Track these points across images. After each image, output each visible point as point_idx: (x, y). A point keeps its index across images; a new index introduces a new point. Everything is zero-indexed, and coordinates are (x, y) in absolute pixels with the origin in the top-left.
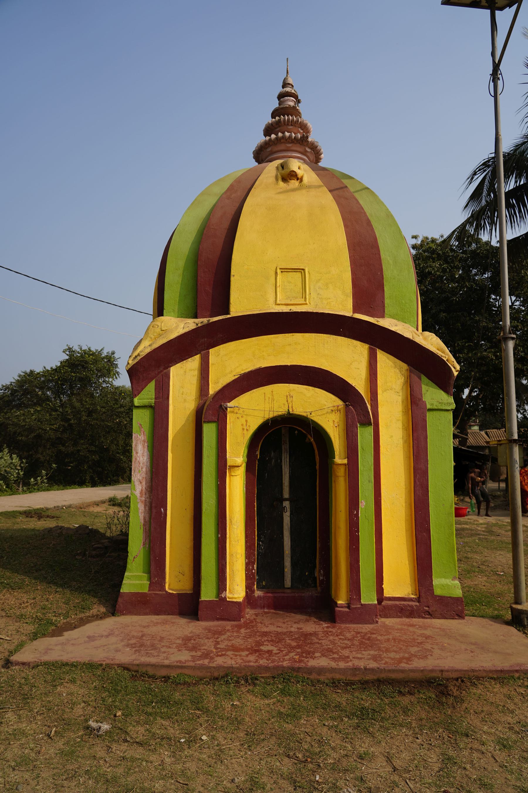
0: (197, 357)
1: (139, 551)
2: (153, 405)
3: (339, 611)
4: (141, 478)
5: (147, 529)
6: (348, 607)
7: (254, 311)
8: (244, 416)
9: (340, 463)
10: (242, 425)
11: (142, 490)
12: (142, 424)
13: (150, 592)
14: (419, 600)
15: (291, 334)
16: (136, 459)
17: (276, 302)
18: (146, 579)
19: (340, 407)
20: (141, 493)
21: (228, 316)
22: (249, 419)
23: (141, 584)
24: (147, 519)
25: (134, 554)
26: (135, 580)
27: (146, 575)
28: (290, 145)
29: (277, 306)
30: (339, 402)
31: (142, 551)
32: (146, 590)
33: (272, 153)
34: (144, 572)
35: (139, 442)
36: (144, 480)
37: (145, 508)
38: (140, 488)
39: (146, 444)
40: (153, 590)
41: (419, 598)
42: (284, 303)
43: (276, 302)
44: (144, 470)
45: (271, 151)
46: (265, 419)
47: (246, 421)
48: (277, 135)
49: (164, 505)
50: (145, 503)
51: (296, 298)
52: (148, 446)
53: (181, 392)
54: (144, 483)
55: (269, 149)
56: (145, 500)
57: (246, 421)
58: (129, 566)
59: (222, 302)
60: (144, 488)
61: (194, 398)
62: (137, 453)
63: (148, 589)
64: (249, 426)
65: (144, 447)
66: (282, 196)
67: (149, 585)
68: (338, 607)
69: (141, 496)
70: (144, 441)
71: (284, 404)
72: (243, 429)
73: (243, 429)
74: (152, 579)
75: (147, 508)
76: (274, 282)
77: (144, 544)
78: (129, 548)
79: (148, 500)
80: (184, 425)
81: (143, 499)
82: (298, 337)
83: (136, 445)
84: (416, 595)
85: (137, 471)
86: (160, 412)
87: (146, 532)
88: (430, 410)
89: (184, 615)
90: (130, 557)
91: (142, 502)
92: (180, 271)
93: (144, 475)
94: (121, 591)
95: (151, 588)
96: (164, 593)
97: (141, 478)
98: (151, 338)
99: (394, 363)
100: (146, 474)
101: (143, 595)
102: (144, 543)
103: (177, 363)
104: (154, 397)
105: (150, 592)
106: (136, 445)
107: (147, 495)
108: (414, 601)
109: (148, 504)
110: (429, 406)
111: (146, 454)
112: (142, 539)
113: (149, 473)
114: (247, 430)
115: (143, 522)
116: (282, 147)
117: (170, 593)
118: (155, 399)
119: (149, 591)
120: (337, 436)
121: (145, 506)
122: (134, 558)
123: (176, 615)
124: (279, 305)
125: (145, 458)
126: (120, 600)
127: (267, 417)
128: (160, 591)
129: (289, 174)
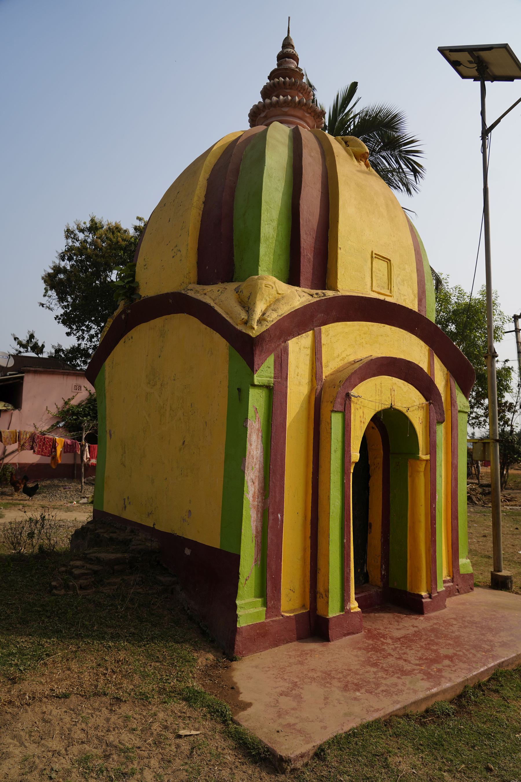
0: (310, 333)
1: (251, 572)
3: (426, 602)
4: (254, 477)
5: (259, 541)
6: (430, 597)
8: (362, 407)
9: (425, 459)
10: (360, 417)
11: (254, 493)
12: (257, 408)
13: (268, 620)
14: (452, 581)
15: (383, 325)
16: (250, 453)
17: (372, 289)
18: (260, 604)
19: (424, 405)
21: (330, 294)
22: (366, 411)
23: (257, 612)
24: (259, 528)
26: (249, 610)
27: (260, 599)
28: (308, 115)
30: (423, 400)
33: (286, 114)
34: (256, 597)
36: (257, 480)
37: (257, 514)
38: (253, 489)
39: (260, 434)
40: (270, 617)
41: (453, 578)
43: (372, 289)
44: (257, 466)
46: (376, 411)
47: (363, 413)
49: (280, 509)
50: (258, 508)
51: (383, 287)
52: (262, 437)
53: (297, 373)
54: (257, 484)
55: (286, 109)
56: (258, 505)
57: (363, 413)
58: (240, 592)
60: (257, 489)
62: (251, 445)
63: (264, 617)
65: (258, 437)
66: (359, 174)
67: (266, 611)
68: (423, 598)
69: (254, 501)
71: (389, 398)
73: (361, 421)
74: (268, 603)
75: (259, 515)
76: (370, 267)
77: (256, 561)
78: (240, 569)
79: (260, 504)
80: (298, 413)
81: (256, 503)
84: (450, 576)
85: (250, 468)
87: (258, 545)
88: (460, 411)
89: (302, 639)
90: (242, 580)
91: (254, 508)
92: (275, 224)
93: (257, 473)
94: (238, 626)
95: (268, 615)
96: (282, 618)
97: (254, 477)
98: (266, 300)
99: (441, 366)
100: (259, 472)
102: (255, 559)
103: (294, 336)
104: (273, 375)
105: (268, 620)
106: (250, 435)
107: (260, 499)
109: (260, 509)
110: (459, 409)
111: (259, 446)
112: (253, 555)
113: (262, 471)
114: (364, 423)
115: (255, 533)
116: (299, 113)
117: (287, 617)
118: (275, 378)
119: (266, 618)
121: (258, 511)
122: (246, 580)
123: (294, 641)
125: (259, 452)
126: (238, 638)
128: (277, 616)
129: (363, 154)
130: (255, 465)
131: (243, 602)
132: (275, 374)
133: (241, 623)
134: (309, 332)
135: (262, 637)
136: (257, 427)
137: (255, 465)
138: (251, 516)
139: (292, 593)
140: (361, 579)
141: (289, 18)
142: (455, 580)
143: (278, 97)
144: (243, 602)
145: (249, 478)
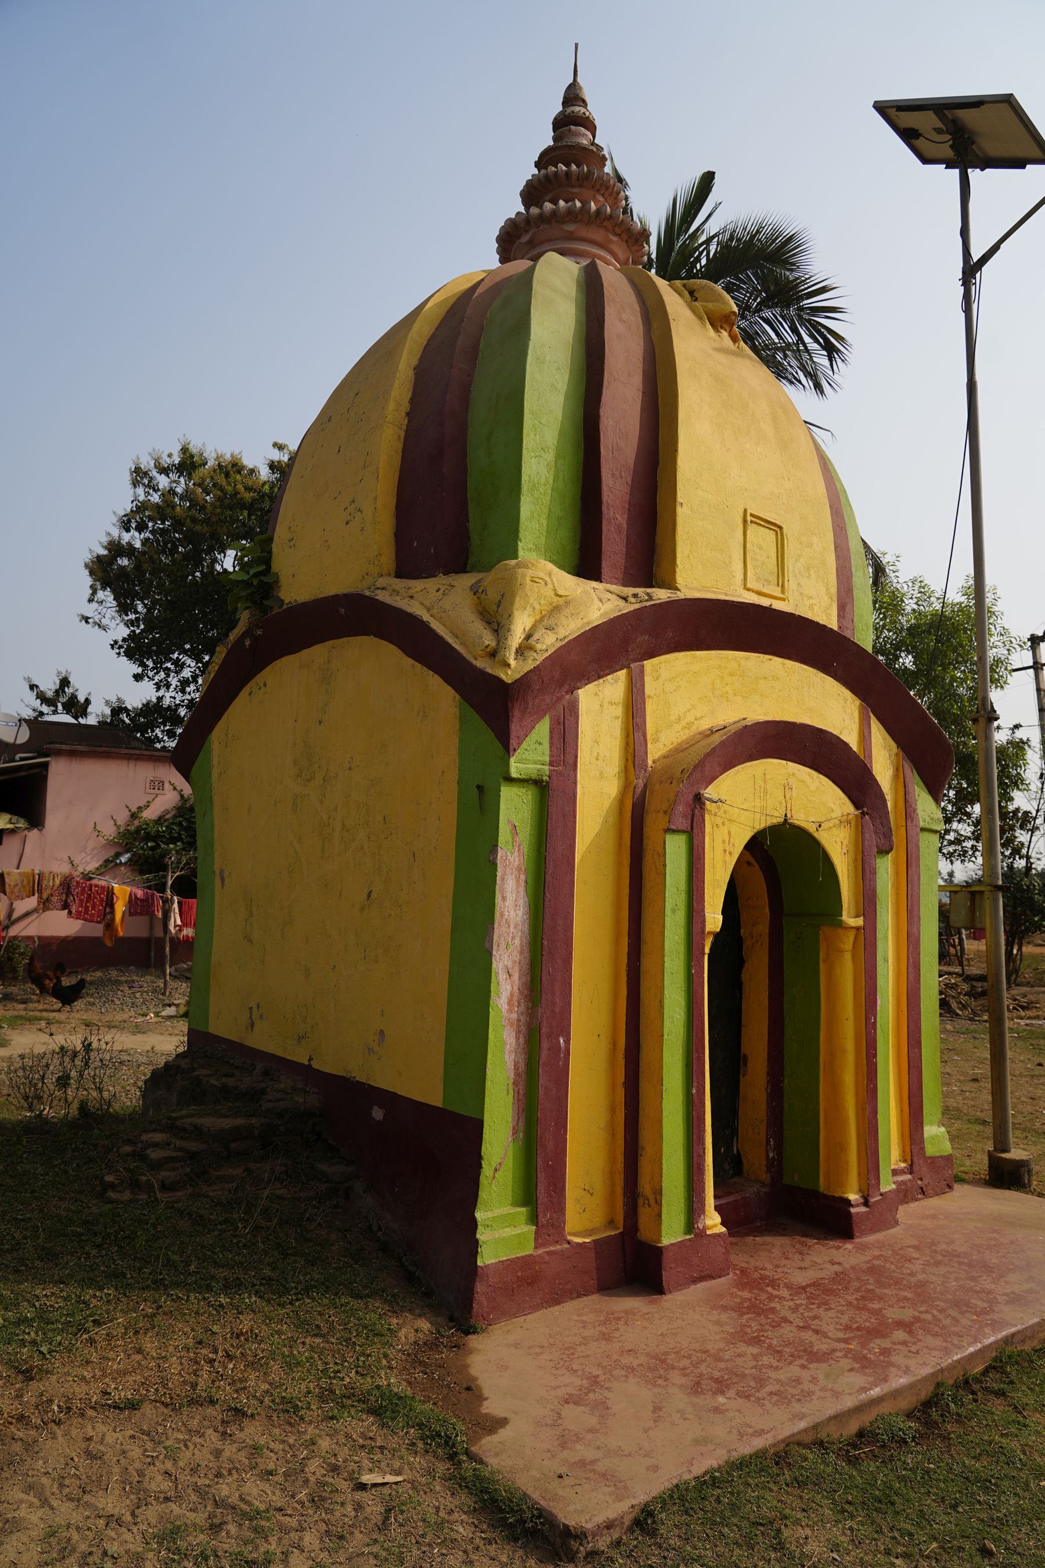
0: (622, 674)
2: (545, 778)
3: (857, 1213)
4: (510, 964)
5: (521, 1092)
6: (866, 1203)
7: (715, 592)
8: (727, 823)
9: (853, 925)
11: (512, 995)
12: (517, 824)
13: (540, 1251)
14: (911, 1170)
15: (768, 657)
16: (502, 915)
17: (745, 584)
19: (850, 817)
20: (510, 1002)
21: (661, 595)
23: (519, 1235)
25: (495, 1161)
26: (501, 1231)
27: (524, 1210)
28: (615, 239)
29: (746, 592)
31: (510, 1153)
32: (529, 1249)
33: (571, 237)
34: (515, 1204)
35: (508, 871)
36: (517, 968)
37: (517, 1038)
38: (509, 988)
39: (523, 877)
40: (543, 1245)
41: (911, 1165)
42: (756, 589)
43: (745, 584)
44: (517, 942)
45: (572, 232)
46: (755, 831)
47: (729, 833)
48: (556, 203)
50: (518, 1026)
53: (595, 754)
54: (516, 977)
55: (570, 227)
56: (519, 1020)
57: (729, 833)
58: (483, 1194)
59: (649, 555)
60: (516, 988)
61: (616, 770)
62: (504, 899)
63: (533, 1244)
64: (733, 845)
67: (536, 1233)
68: (852, 1206)
69: (510, 1011)
70: (519, 869)
71: (781, 803)
72: (725, 851)
73: (725, 851)
74: (540, 1218)
75: (522, 1040)
77: (515, 1132)
78: (483, 1148)
79: (522, 1018)
80: (598, 835)
81: (515, 1016)
82: (776, 663)
83: (503, 879)
84: (905, 1161)
85: (503, 945)
86: (554, 796)
87: (519, 1100)
88: (923, 830)
89: (609, 1288)
90: (487, 1170)
94: (479, 1263)
95: (540, 1241)
96: (567, 1246)
97: (510, 964)
98: (534, 609)
99: (884, 739)
100: (521, 953)
101: (525, 1262)
102: (514, 1128)
104: (547, 759)
105: (540, 1251)
106: (503, 879)
107: (522, 1008)
108: (905, 1173)
109: (523, 1028)
110: (922, 824)
111: (521, 902)
112: (510, 1119)
113: (526, 950)
114: (730, 853)
116: (598, 235)
117: (578, 1244)
118: (551, 764)
120: (846, 872)
121: (518, 1032)
123: (593, 1293)
124: (749, 590)
125: (520, 913)
126: (480, 1287)
127: (760, 826)
128: (557, 1242)
130: (513, 938)
131: (490, 1214)
132: (551, 756)
133: (487, 1257)
134: (619, 673)
135: (528, 1284)
136: (517, 863)
137: (513, 938)
138: (505, 1043)
139: (588, 1195)
140: (727, 1168)
141: (577, 45)
142: (916, 1168)
143: (555, 202)
144: (490, 1214)
145: (501, 966)
